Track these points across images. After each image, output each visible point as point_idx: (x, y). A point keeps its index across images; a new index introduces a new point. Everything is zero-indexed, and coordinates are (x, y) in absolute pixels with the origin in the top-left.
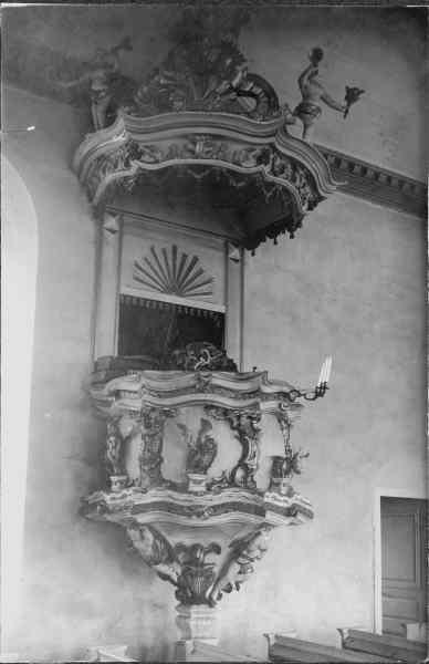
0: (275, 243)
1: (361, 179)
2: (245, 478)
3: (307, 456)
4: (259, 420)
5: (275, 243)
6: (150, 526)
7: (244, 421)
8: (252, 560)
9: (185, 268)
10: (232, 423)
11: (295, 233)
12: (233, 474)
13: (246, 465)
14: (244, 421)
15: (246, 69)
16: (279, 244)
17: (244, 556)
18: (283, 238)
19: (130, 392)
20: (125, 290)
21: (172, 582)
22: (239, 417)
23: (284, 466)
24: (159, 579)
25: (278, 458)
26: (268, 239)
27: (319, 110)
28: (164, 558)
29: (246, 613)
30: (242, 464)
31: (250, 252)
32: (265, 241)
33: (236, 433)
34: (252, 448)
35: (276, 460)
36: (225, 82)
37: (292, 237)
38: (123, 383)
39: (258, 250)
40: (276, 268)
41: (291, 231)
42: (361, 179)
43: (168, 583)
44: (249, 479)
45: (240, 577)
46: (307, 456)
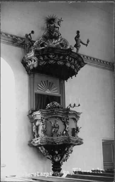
0: (72, 78)
1: (94, 61)
2: (66, 133)
3: (81, 128)
4: (68, 120)
5: (67, 81)
6: (51, 59)
7: (65, 120)
8: (69, 153)
9: (42, 90)
10: (62, 120)
11: (76, 76)
12: (63, 133)
13: (66, 130)
14: (65, 120)
15: (61, 37)
16: (76, 77)
17: (67, 153)
18: (74, 77)
19: (38, 115)
20: (35, 91)
21: (50, 159)
22: (64, 119)
23: (76, 130)
24: (47, 159)
25: (74, 129)
26: (70, 77)
27: (80, 45)
28: (48, 154)
29: (68, 168)
30: (65, 130)
31: (66, 81)
32: (69, 78)
33: (63, 123)
34: (67, 126)
35: (73, 129)
36: (57, 40)
37: (75, 76)
38: (35, 113)
39: (68, 80)
40: (70, 85)
41: (75, 75)
42: (94, 61)
43: (49, 159)
44: (67, 133)
45: (66, 158)
46: (81, 128)
